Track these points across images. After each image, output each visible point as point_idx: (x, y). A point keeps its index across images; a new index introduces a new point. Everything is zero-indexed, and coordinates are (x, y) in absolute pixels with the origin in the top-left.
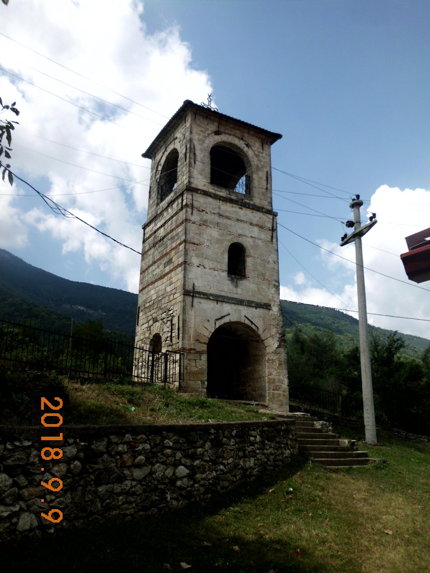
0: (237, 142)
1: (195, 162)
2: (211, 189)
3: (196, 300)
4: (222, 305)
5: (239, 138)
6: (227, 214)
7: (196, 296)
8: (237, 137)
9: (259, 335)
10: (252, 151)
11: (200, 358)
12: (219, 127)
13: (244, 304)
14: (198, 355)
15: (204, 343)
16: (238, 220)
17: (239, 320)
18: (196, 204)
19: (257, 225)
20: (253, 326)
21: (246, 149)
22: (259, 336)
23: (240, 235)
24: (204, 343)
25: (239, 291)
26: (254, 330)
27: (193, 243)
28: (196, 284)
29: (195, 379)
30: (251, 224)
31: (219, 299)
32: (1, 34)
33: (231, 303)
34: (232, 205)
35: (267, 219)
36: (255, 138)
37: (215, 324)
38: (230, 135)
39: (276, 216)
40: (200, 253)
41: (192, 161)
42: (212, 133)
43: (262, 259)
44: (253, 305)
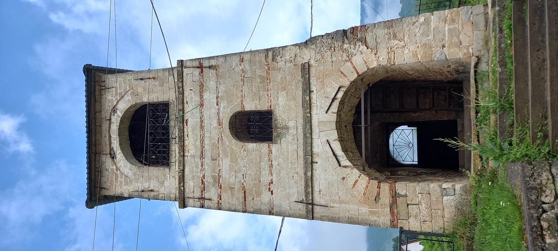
0: (115, 127)
1: (152, 191)
2: (175, 167)
3: (318, 199)
4: (318, 155)
5: (110, 124)
6: (198, 143)
7: (312, 200)
8: (110, 127)
9: (351, 83)
10: (120, 101)
11: (403, 196)
12: (106, 154)
13: (309, 115)
14: (399, 200)
15: (379, 187)
16: (202, 127)
17: (334, 126)
18: (198, 194)
19: (201, 97)
20: (340, 95)
21: (120, 114)
22: (353, 83)
23: (220, 123)
24: (379, 187)
25: (291, 124)
26: (346, 93)
27: (245, 200)
28: (295, 198)
29: (440, 207)
30: (202, 105)
31: (310, 160)
32: (276, 250)
33: (312, 139)
34: (186, 138)
35: (191, 76)
36: (103, 101)
37: (345, 167)
38: (110, 136)
39: (182, 61)
40: (254, 189)
41: (152, 194)
42: (115, 164)
43: (242, 83)
44: (308, 98)
